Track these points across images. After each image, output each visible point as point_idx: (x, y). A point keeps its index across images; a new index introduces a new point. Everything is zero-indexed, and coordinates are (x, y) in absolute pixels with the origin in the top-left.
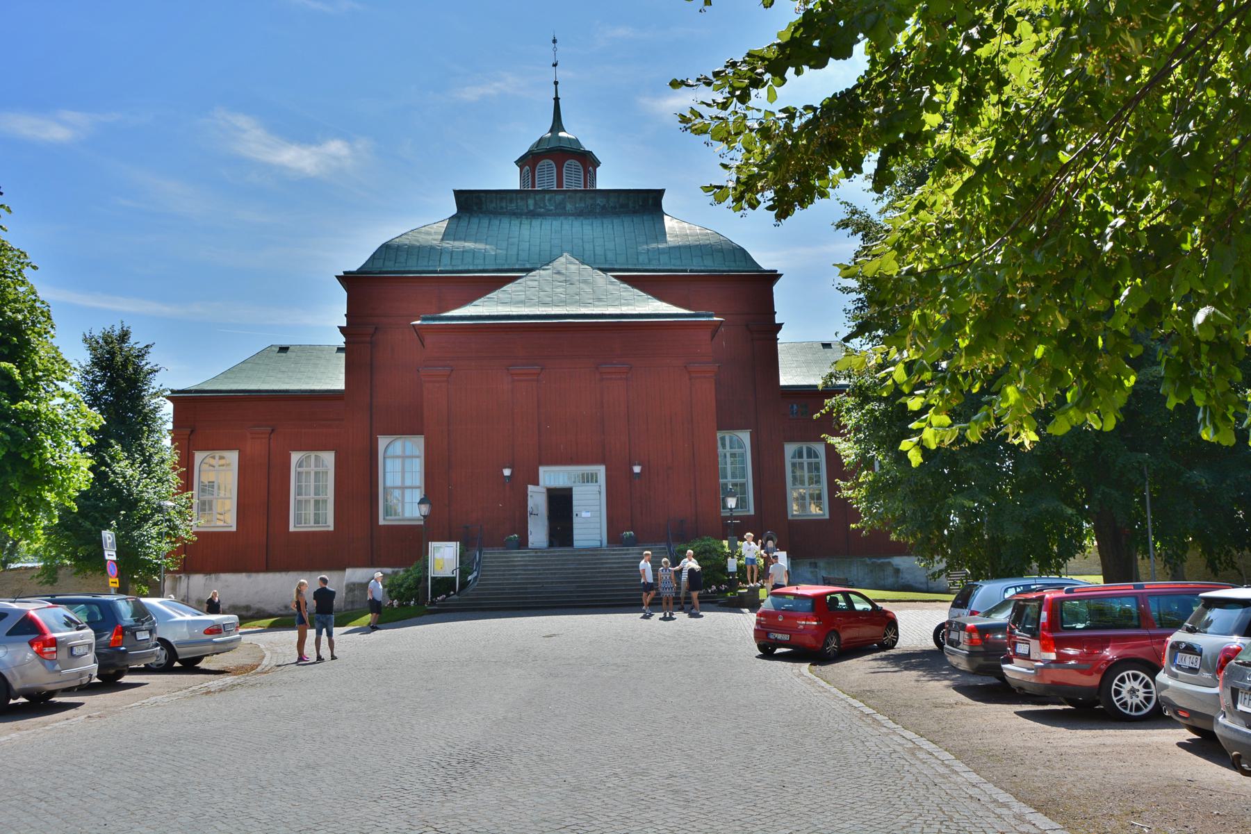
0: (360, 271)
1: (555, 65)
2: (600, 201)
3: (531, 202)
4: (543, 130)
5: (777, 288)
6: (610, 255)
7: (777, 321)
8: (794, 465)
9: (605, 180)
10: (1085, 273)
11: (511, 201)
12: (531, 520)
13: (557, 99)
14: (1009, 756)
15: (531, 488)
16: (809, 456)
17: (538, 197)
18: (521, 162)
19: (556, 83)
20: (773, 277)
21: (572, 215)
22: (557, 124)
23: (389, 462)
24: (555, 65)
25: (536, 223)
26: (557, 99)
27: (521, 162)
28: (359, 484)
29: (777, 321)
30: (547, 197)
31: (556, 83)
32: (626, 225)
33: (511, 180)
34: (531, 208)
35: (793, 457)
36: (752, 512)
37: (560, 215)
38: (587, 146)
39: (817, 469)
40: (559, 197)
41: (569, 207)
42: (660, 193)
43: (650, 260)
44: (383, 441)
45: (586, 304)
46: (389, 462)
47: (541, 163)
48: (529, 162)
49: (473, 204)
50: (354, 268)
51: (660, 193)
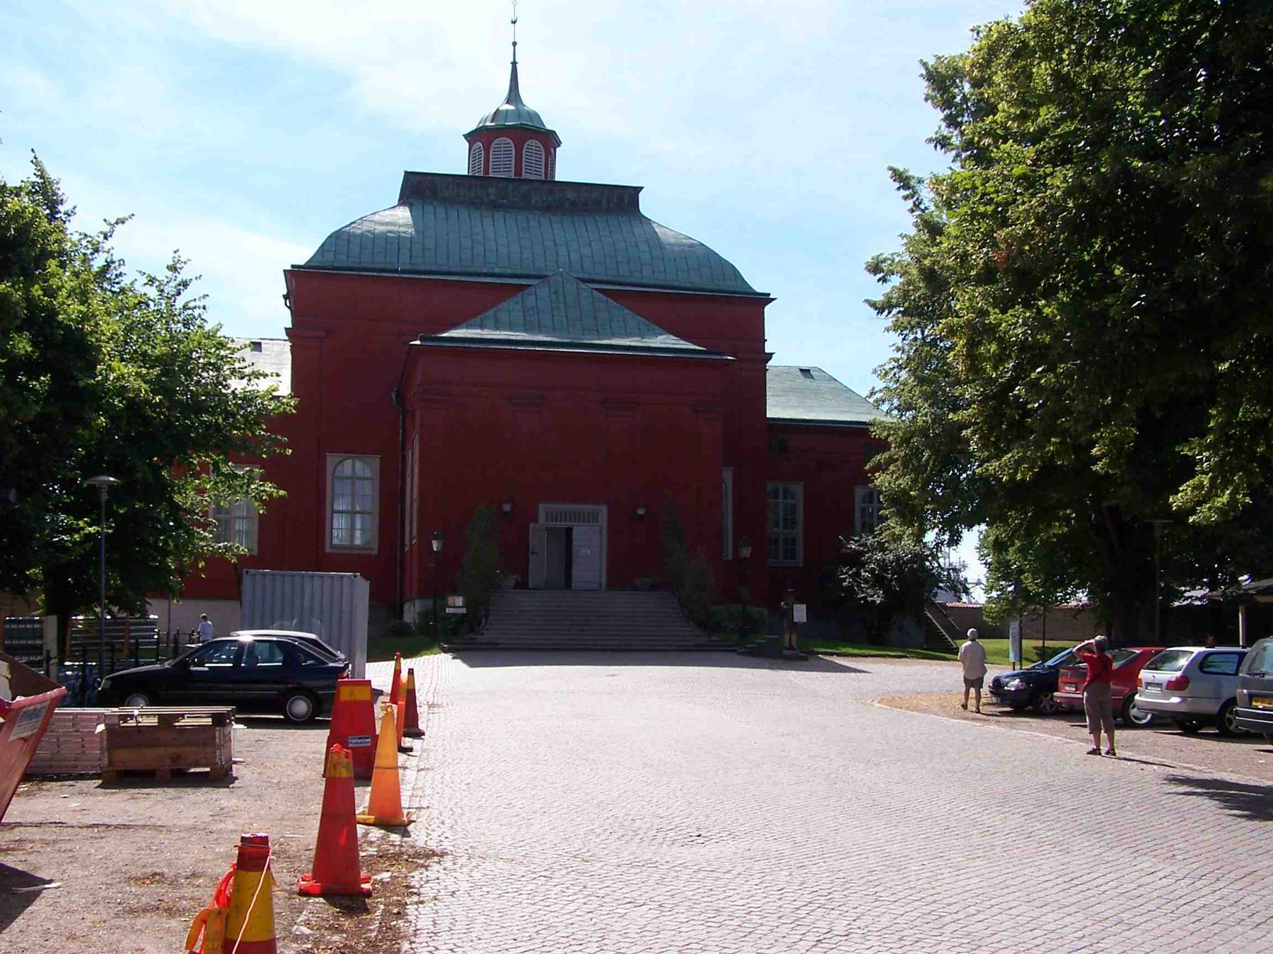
1: (514, 22)
5: (767, 309)
6: (587, 264)
7: (767, 351)
8: (863, 510)
9: (567, 169)
10: (1129, 147)
12: (532, 558)
13: (514, 64)
15: (532, 525)
16: (785, 497)
17: (501, 185)
18: (471, 137)
19: (515, 44)
20: (766, 299)
21: (537, 209)
22: (514, 94)
23: (338, 486)
24: (514, 22)
25: (499, 216)
26: (514, 64)
27: (471, 137)
29: (767, 351)
30: (511, 186)
31: (515, 44)
32: (533, 224)
33: (454, 160)
34: (492, 197)
35: (864, 501)
36: (541, 506)
37: (523, 208)
40: (525, 188)
41: (535, 198)
42: (639, 189)
43: (631, 272)
44: (331, 459)
45: (612, 336)
46: (336, 483)
47: (497, 141)
48: (480, 138)
49: (419, 189)
51: (639, 189)
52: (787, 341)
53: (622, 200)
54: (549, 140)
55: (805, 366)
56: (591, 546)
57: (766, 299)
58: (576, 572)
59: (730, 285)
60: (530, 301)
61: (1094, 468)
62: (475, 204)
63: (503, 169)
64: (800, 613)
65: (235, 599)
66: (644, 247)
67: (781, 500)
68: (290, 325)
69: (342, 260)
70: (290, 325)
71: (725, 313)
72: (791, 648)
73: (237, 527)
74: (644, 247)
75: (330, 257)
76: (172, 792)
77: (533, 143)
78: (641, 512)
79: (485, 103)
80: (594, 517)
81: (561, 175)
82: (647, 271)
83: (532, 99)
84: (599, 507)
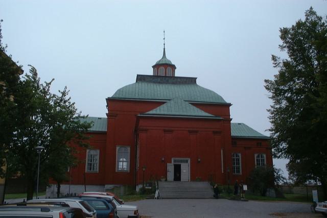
0: (112, 97)
2: (179, 80)
3: (159, 79)
4: (160, 57)
5: (230, 107)
7: (231, 118)
8: (257, 160)
9: (178, 74)
11: (154, 79)
12: (168, 173)
13: (164, 49)
14: (86, 205)
18: (154, 67)
20: (230, 105)
25: (161, 85)
26: (164, 49)
27: (154, 67)
28: (108, 160)
29: (231, 118)
31: (53, 79)
33: (150, 72)
37: (166, 83)
38: (173, 63)
39: (239, 160)
40: (167, 78)
41: (170, 81)
42: (196, 78)
44: (118, 148)
48: (156, 67)
49: (140, 78)
50: (110, 97)
51: (196, 78)
52: (236, 116)
53: (192, 81)
54: (173, 67)
55: (239, 123)
56: (186, 170)
57: (230, 105)
58: (168, 179)
59: (220, 101)
60: (169, 104)
61: (14, 133)
62: (150, 82)
63: (162, 72)
64: (245, 188)
65: (82, 184)
66: (198, 92)
67: (260, 158)
68: (107, 112)
69: (121, 96)
70: (107, 112)
71: (221, 109)
72: (243, 198)
73: (125, 164)
74: (198, 92)
75: (115, 96)
76: (291, 202)
77: (169, 69)
78: (199, 160)
79: (157, 58)
80: (187, 161)
81: (177, 75)
82: (193, 98)
83: (168, 57)
84: (187, 159)
